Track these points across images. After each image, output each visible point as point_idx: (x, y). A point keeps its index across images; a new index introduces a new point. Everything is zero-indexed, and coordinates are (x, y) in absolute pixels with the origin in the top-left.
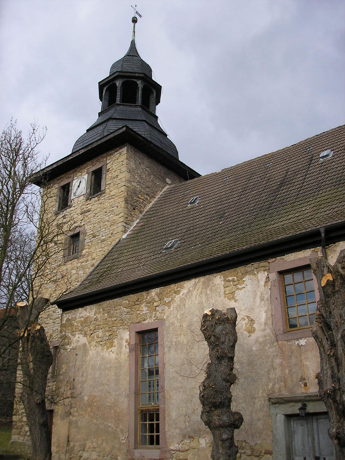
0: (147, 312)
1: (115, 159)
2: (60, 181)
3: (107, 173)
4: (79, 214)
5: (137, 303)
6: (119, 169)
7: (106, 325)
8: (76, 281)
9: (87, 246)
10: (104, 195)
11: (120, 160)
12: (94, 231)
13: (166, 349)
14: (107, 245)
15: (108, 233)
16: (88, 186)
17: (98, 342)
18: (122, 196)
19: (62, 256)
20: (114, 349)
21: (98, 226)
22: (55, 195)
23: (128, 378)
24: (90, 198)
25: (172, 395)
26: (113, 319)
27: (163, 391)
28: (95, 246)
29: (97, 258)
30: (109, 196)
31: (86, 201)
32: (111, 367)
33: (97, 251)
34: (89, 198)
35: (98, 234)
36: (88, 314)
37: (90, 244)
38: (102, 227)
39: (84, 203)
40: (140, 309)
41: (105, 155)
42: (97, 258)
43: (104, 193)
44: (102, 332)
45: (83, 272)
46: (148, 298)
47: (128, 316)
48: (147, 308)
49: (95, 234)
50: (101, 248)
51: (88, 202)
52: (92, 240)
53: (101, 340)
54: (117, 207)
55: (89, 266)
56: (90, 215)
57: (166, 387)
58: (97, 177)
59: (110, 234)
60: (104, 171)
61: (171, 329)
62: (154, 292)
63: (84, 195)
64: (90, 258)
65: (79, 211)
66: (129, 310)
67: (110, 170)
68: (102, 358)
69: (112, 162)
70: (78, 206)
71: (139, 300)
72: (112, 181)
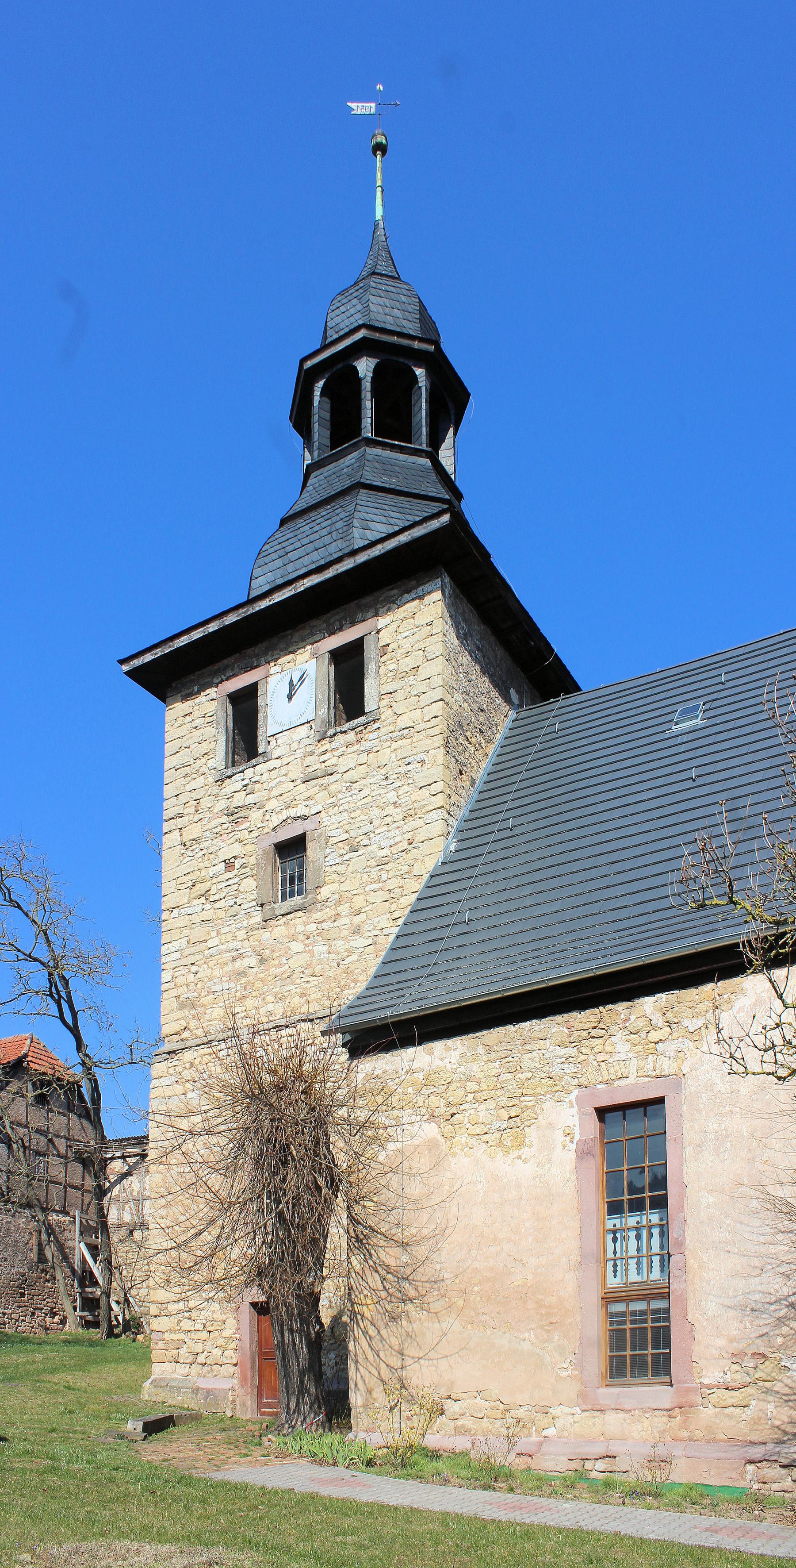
0: (630, 1055)
1: (404, 615)
2: (224, 678)
3: (382, 659)
4: (299, 782)
5: (594, 1033)
6: (422, 646)
7: (499, 1093)
8: (306, 971)
9: (335, 876)
10: (376, 726)
11: (421, 619)
12: (353, 833)
13: (689, 1151)
14: (399, 873)
15: (397, 839)
16: (320, 697)
17: (474, 1136)
18: (436, 731)
19: (254, 903)
20: (526, 1152)
21: (363, 817)
22: (211, 719)
23: (575, 1224)
24: (331, 732)
25: (705, 1259)
26: (520, 1075)
27: (681, 1251)
28: (359, 875)
29: (367, 909)
30: (391, 728)
31: (319, 741)
32: (521, 1198)
33: (367, 889)
34: (326, 732)
35: (366, 842)
36: (438, 1062)
37: (341, 869)
38: (376, 823)
39: (312, 747)
40: (608, 1048)
41: (368, 599)
42: (367, 909)
43: (374, 721)
44: (487, 1110)
45: (326, 948)
46: (632, 1020)
47: (570, 1069)
48: (628, 1046)
49: (357, 840)
50: (379, 881)
51: (326, 745)
52: (346, 857)
53: (486, 1130)
54: (422, 762)
55: (345, 933)
56: (336, 784)
57: (688, 1242)
58: (349, 666)
59: (406, 843)
60: (370, 652)
61: (705, 1099)
62: (649, 1004)
63: (308, 722)
64: (344, 909)
65: (296, 772)
66: (570, 1051)
67: (390, 649)
68: (492, 1174)
69: (394, 625)
70: (292, 758)
71: (601, 1025)
72: (401, 683)
